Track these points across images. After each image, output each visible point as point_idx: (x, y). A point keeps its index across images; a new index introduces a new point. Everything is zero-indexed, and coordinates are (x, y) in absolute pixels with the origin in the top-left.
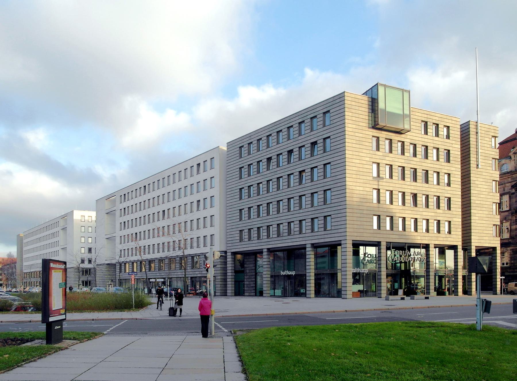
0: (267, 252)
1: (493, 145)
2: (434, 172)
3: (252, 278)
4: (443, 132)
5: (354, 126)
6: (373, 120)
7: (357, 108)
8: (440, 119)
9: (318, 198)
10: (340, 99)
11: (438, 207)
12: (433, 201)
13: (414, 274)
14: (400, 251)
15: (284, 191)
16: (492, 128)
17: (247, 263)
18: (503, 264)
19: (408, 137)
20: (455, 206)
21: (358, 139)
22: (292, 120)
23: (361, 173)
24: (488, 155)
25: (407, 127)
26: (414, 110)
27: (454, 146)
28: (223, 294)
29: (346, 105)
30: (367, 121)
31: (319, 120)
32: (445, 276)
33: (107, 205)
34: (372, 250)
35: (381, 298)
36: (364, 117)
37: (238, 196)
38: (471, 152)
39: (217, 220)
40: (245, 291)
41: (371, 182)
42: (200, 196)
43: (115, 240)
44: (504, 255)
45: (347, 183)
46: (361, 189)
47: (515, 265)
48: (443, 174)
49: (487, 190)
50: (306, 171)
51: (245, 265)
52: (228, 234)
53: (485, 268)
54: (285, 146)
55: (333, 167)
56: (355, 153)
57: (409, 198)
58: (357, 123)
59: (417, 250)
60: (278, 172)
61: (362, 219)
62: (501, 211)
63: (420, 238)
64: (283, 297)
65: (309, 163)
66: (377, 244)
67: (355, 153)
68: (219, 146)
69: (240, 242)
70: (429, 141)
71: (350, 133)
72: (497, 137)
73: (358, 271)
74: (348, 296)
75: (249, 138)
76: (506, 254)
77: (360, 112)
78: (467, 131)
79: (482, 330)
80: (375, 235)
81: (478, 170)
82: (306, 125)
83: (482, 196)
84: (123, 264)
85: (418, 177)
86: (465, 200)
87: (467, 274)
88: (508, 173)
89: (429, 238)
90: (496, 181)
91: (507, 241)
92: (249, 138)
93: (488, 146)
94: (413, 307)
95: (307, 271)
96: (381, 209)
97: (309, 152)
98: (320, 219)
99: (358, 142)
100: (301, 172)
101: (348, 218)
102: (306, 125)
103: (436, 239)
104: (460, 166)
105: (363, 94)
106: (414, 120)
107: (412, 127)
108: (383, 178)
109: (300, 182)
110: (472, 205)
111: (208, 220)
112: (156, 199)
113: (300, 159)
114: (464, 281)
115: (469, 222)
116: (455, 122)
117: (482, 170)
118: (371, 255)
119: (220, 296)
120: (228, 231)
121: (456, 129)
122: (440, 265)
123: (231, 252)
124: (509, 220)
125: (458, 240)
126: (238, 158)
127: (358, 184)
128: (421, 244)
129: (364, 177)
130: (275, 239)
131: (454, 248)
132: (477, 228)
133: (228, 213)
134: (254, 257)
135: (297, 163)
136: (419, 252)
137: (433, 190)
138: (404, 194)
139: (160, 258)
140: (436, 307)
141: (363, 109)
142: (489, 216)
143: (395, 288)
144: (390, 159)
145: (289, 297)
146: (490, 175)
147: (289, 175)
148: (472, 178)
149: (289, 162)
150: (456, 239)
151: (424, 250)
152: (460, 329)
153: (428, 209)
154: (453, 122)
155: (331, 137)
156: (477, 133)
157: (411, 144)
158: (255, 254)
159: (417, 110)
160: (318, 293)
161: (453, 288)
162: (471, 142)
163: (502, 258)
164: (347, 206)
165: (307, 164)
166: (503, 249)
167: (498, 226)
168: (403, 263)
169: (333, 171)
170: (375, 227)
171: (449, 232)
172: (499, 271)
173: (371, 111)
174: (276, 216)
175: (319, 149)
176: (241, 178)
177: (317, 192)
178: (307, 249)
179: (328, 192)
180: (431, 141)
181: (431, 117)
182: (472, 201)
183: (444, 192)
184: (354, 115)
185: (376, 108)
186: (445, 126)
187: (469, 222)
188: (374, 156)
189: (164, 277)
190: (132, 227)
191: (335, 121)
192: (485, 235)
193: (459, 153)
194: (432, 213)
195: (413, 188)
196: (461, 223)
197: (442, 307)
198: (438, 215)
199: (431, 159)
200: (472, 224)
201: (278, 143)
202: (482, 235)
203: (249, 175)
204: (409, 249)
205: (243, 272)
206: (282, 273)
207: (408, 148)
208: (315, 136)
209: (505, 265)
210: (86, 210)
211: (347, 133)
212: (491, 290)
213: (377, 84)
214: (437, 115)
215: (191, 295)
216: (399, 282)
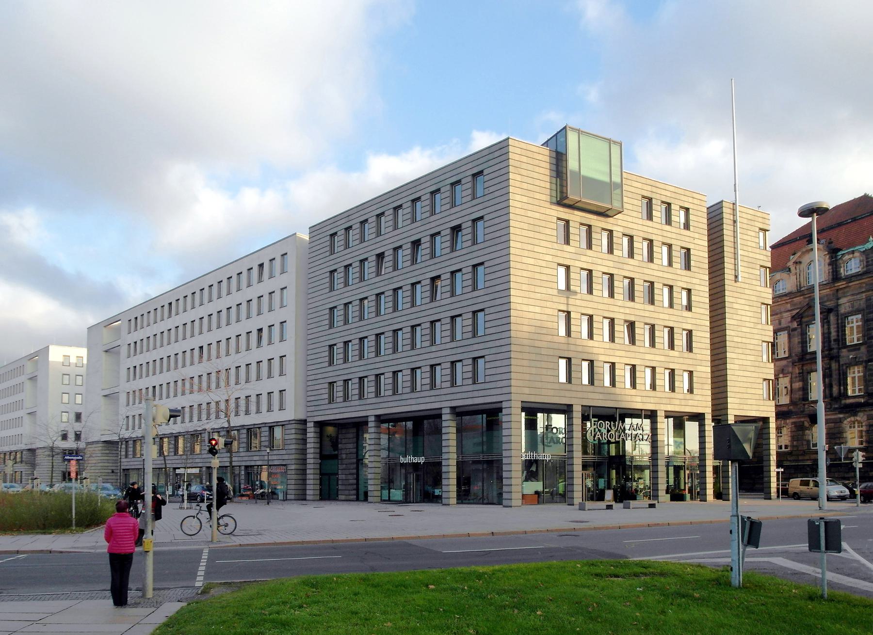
1: (762, 244)
2: (664, 285)
3: (352, 468)
4: (679, 217)
5: (525, 199)
6: (559, 190)
7: (530, 167)
8: (673, 195)
9: (463, 325)
10: (500, 151)
11: (672, 346)
12: (662, 336)
14: (607, 422)
15: (404, 312)
16: (759, 214)
17: (344, 441)
18: (780, 447)
19: (620, 222)
20: (699, 345)
21: (531, 221)
22: (418, 188)
23: (538, 283)
24: (753, 261)
25: (616, 205)
26: (629, 177)
27: (696, 241)
28: (302, 497)
29: (511, 162)
30: (548, 192)
31: (465, 187)
32: (684, 466)
33: (106, 338)
34: (558, 421)
35: (573, 505)
36: (543, 184)
37: (327, 322)
38: (726, 254)
39: (290, 365)
40: (340, 492)
41: (555, 299)
42: (262, 322)
43: (118, 399)
44: (781, 433)
45: (513, 299)
46: (538, 310)
47: (800, 449)
48: (679, 290)
49: (753, 320)
50: (443, 277)
51: (339, 445)
52: (309, 388)
53: (748, 448)
54: (407, 233)
55: (488, 271)
56: (526, 247)
57: (621, 330)
58: (531, 194)
59: (636, 421)
60: (395, 279)
61: (538, 364)
62: (775, 359)
63: (638, 400)
64: (404, 503)
66: (566, 410)
67: (526, 247)
68: (296, 234)
69: (330, 403)
70: (655, 231)
71: (518, 211)
72: (768, 231)
73: (533, 458)
74: (514, 503)
75: (346, 219)
76: (785, 431)
77: (536, 175)
78: (717, 218)
79: (743, 586)
80: (562, 393)
81: (738, 284)
82: (443, 196)
83: (744, 329)
84: (131, 442)
85: (636, 294)
86: (716, 335)
87: (721, 464)
88: (786, 295)
89: (656, 400)
90: (767, 305)
91: (785, 409)
92: (346, 219)
93: (754, 245)
94: (621, 525)
95: (444, 456)
96: (572, 348)
97: (448, 244)
98: (465, 362)
99: (531, 227)
100: (434, 279)
101: (513, 362)
102: (443, 196)
103: (667, 401)
104: (707, 278)
105: (542, 145)
106: (630, 195)
107: (625, 205)
108: (575, 293)
109: (433, 297)
110: (728, 344)
111: (276, 363)
112: (189, 326)
113: (433, 255)
114: (717, 475)
115: (723, 373)
116: (698, 202)
117: (743, 285)
118: (557, 429)
119: (295, 500)
120: (310, 383)
121: (699, 214)
122: (677, 448)
123: (314, 422)
124: (788, 373)
125: (704, 404)
126: (328, 254)
127: (531, 302)
128: (642, 410)
129: (543, 290)
130: (390, 399)
131: (698, 417)
132: (737, 384)
133: (310, 352)
134: (354, 430)
135: (428, 263)
136: (640, 423)
137: (662, 316)
138: (612, 321)
139: (195, 431)
140: (663, 525)
141: (542, 170)
142: (757, 364)
143: (600, 487)
144: (589, 259)
145: (413, 503)
147: (413, 285)
148: (727, 299)
149: (414, 260)
150: (702, 403)
151: (648, 421)
152: (698, 583)
153: (654, 349)
154: (695, 201)
155: (486, 218)
156: (735, 222)
157: (624, 235)
158: (359, 425)
159: (634, 178)
160: (464, 496)
161: (698, 488)
162: (725, 238)
163: (778, 437)
164: (513, 341)
165: (443, 265)
166: (779, 422)
167: (771, 381)
168: (613, 443)
169: (488, 277)
170: (563, 378)
171: (691, 390)
172: (773, 458)
173: (554, 174)
174: (391, 357)
175: (465, 238)
176: (332, 289)
177: (460, 315)
178: (444, 417)
179: (480, 315)
180: (659, 232)
181: (659, 191)
182: (728, 338)
183: (682, 320)
184: (525, 179)
185: (564, 170)
186: (681, 207)
187: (723, 373)
188: (559, 253)
189: (200, 465)
190: (148, 375)
191: (492, 189)
192: (749, 396)
193: (706, 255)
194: (661, 357)
195: (627, 311)
196: (709, 376)
197: (675, 524)
198: (672, 360)
199: (659, 262)
200: (729, 378)
201: (396, 228)
202: (746, 396)
203: (346, 284)
204: (622, 418)
205: (336, 457)
206: (402, 460)
207: (620, 241)
208: (458, 215)
209: (783, 449)
210: (74, 346)
211: (512, 210)
212: (761, 490)
213: (565, 128)
214: (667, 187)
215: (244, 498)
216: (606, 476)
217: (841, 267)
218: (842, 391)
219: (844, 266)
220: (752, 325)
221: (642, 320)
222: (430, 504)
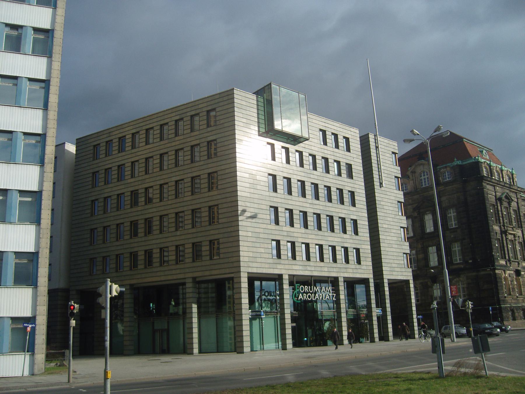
0: (192, 282)
13: (322, 317)
14: (306, 286)
22: (166, 117)
24: (390, 173)
27: (355, 160)
65: (189, 171)
75: (108, 135)
81: (382, 188)
89: (337, 270)
117: (386, 189)
131: (365, 282)
142: (399, 243)
146: (395, 195)
165: (186, 172)
198: (345, 241)
207: (307, 159)
217: (440, 177)
218: (449, 260)
219: (442, 176)
220: (393, 216)
221: (325, 212)
222: (151, 358)
